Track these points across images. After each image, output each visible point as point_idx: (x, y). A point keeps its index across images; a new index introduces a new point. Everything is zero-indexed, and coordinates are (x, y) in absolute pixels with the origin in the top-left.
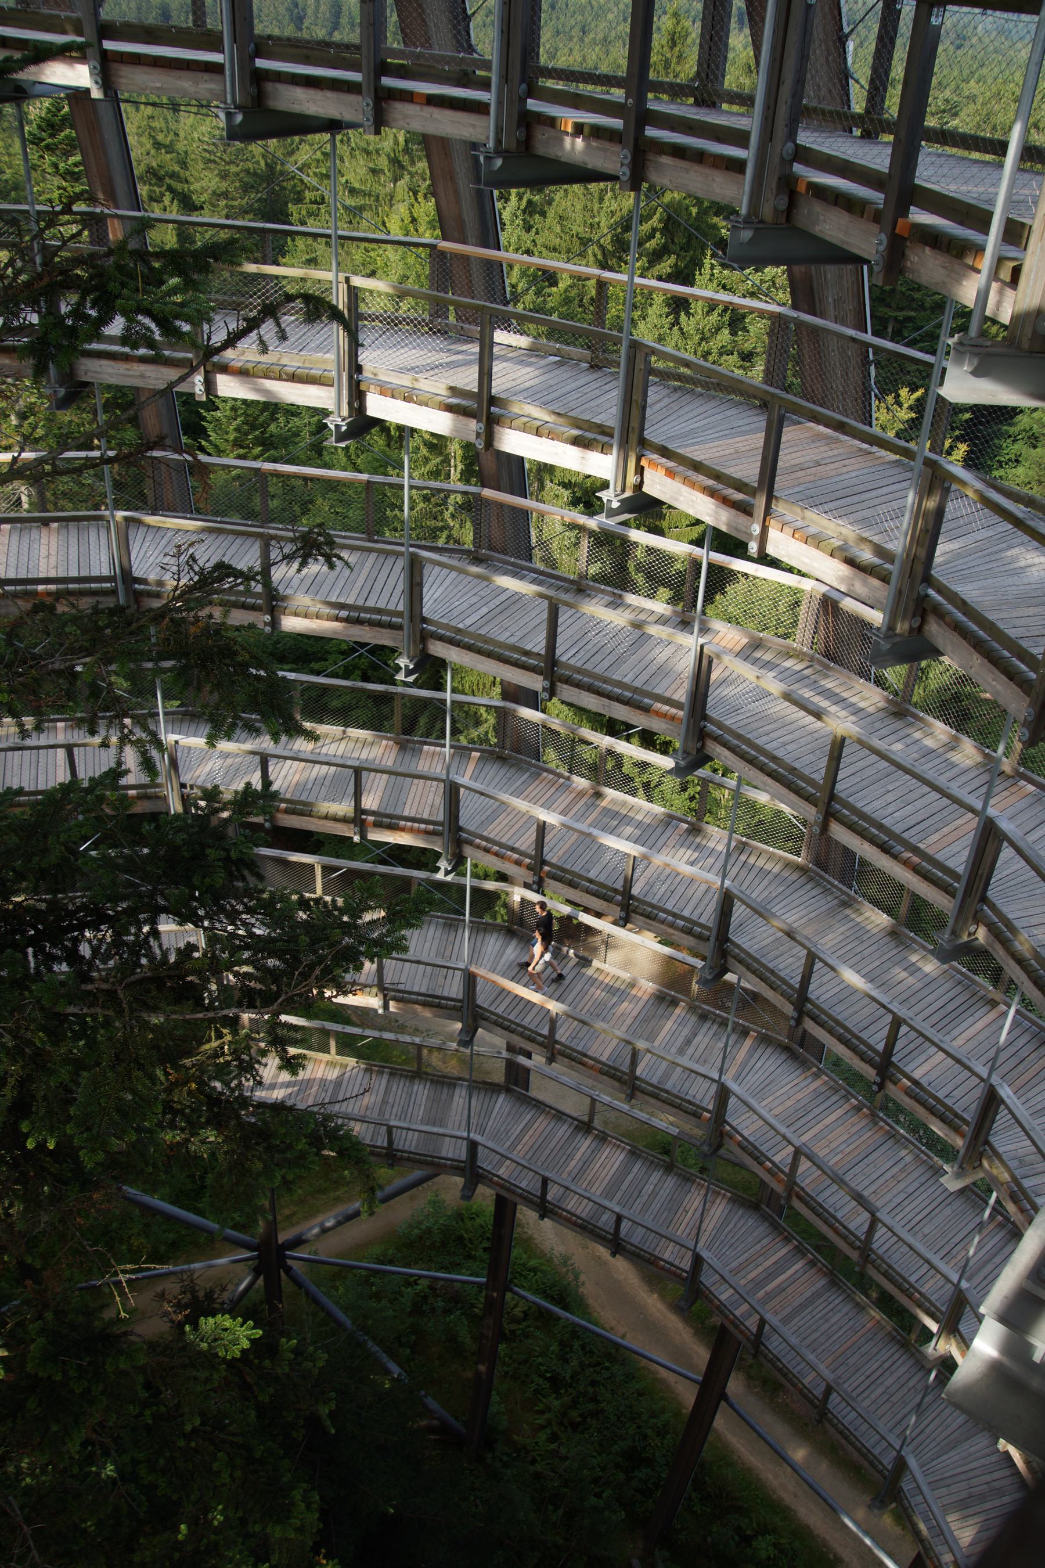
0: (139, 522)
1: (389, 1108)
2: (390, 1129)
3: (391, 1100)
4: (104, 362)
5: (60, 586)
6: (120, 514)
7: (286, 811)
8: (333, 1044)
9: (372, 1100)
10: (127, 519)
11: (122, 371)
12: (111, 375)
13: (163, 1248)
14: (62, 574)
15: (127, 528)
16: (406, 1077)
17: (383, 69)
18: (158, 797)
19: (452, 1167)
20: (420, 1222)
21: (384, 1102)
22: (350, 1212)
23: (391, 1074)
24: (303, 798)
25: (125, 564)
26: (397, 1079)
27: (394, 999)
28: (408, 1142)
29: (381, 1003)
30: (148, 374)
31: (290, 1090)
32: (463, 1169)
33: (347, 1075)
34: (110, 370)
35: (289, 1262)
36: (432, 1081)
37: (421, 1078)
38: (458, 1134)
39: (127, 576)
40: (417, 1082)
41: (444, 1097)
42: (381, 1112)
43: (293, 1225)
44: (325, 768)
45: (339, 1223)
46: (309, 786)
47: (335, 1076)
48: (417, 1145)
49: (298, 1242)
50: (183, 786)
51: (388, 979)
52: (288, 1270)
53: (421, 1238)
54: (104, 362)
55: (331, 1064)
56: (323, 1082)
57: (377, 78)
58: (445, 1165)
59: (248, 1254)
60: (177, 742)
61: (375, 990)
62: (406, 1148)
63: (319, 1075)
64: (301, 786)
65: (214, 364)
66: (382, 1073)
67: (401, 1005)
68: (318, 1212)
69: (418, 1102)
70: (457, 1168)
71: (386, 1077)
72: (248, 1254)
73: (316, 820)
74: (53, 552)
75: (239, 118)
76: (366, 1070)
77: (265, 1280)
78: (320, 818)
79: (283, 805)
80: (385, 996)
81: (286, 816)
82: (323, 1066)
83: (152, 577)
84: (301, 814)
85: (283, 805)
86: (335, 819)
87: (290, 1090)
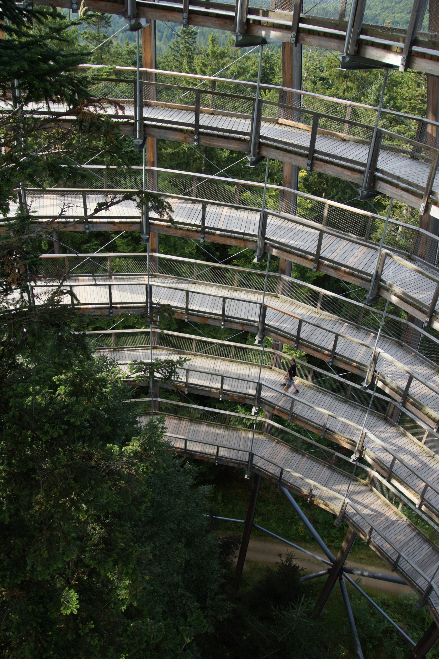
0: (391, 257)
1: (407, 546)
2: (399, 556)
3: (410, 544)
4: (388, 185)
5: (351, 271)
6: (385, 251)
7: (411, 403)
8: (401, 505)
9: (403, 539)
10: (387, 254)
11: (394, 191)
12: (389, 192)
13: (308, 537)
14: (355, 267)
15: (386, 257)
16: (424, 539)
17: (415, 42)
18: (363, 371)
19: (418, 590)
20: (410, 600)
21: (407, 543)
22: (376, 575)
23: (418, 533)
24: (421, 402)
25: (379, 272)
26: (419, 537)
27: (425, 505)
28: (404, 566)
29: (419, 503)
30: (404, 196)
31: (372, 513)
32: (422, 594)
33: (399, 522)
34: (389, 189)
35: (343, 576)
36: (433, 548)
37: (429, 544)
38: (427, 578)
39: (378, 277)
40: (427, 544)
41: (434, 558)
42: (403, 546)
43: (361, 563)
44: (434, 393)
45: (369, 576)
46: (428, 397)
47: (394, 519)
48: (408, 570)
49: (350, 571)
50: (375, 371)
51: (426, 497)
52: (341, 579)
53: (407, 606)
54: (388, 185)
55: (396, 514)
56: (388, 518)
57: (411, 46)
58: (415, 586)
59: (329, 562)
60: (379, 353)
61: (419, 496)
62: (403, 568)
63: (388, 515)
64: (424, 396)
65: (432, 200)
66: (414, 530)
67: (427, 509)
68: (374, 565)
69: (421, 552)
70: (420, 592)
71: (415, 533)
72: (329, 562)
73: (422, 414)
74: (359, 256)
75: (348, 59)
76: (408, 525)
77: (329, 577)
78: (423, 413)
79: (411, 400)
80: (422, 502)
81: (410, 405)
82: (392, 512)
83: (388, 282)
84: (417, 407)
85: (411, 400)
86: (430, 417)
87: (372, 513)
